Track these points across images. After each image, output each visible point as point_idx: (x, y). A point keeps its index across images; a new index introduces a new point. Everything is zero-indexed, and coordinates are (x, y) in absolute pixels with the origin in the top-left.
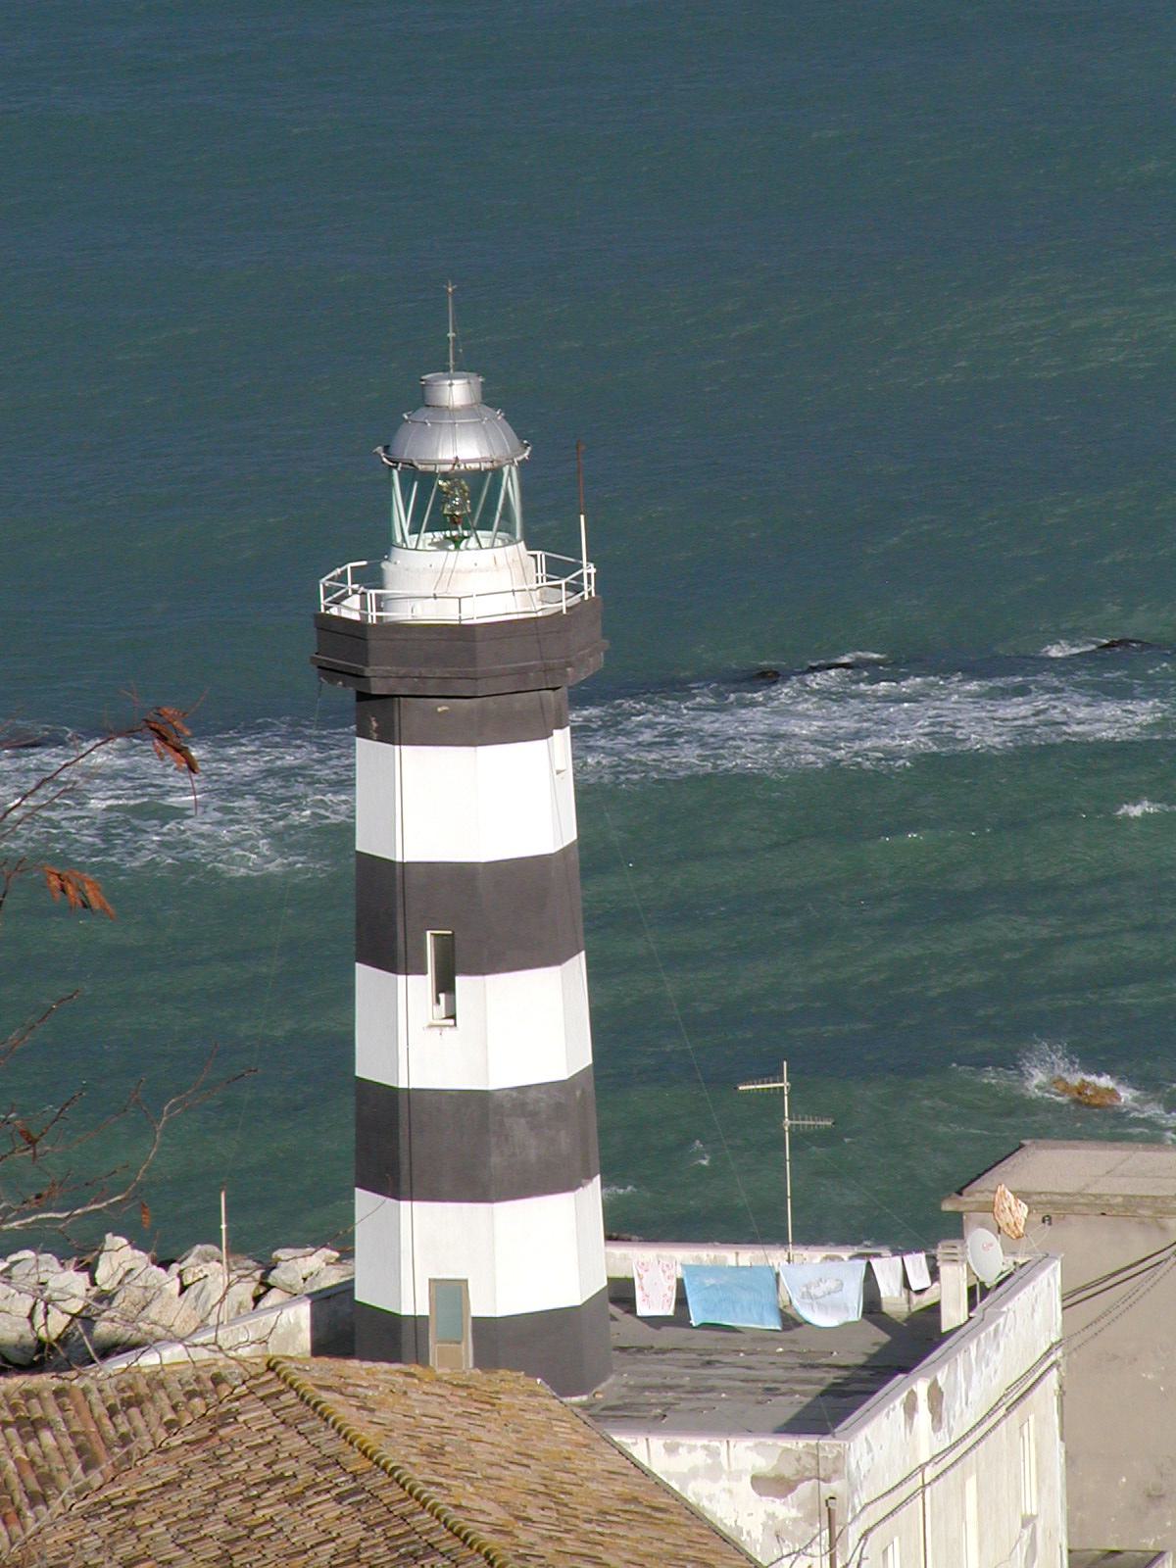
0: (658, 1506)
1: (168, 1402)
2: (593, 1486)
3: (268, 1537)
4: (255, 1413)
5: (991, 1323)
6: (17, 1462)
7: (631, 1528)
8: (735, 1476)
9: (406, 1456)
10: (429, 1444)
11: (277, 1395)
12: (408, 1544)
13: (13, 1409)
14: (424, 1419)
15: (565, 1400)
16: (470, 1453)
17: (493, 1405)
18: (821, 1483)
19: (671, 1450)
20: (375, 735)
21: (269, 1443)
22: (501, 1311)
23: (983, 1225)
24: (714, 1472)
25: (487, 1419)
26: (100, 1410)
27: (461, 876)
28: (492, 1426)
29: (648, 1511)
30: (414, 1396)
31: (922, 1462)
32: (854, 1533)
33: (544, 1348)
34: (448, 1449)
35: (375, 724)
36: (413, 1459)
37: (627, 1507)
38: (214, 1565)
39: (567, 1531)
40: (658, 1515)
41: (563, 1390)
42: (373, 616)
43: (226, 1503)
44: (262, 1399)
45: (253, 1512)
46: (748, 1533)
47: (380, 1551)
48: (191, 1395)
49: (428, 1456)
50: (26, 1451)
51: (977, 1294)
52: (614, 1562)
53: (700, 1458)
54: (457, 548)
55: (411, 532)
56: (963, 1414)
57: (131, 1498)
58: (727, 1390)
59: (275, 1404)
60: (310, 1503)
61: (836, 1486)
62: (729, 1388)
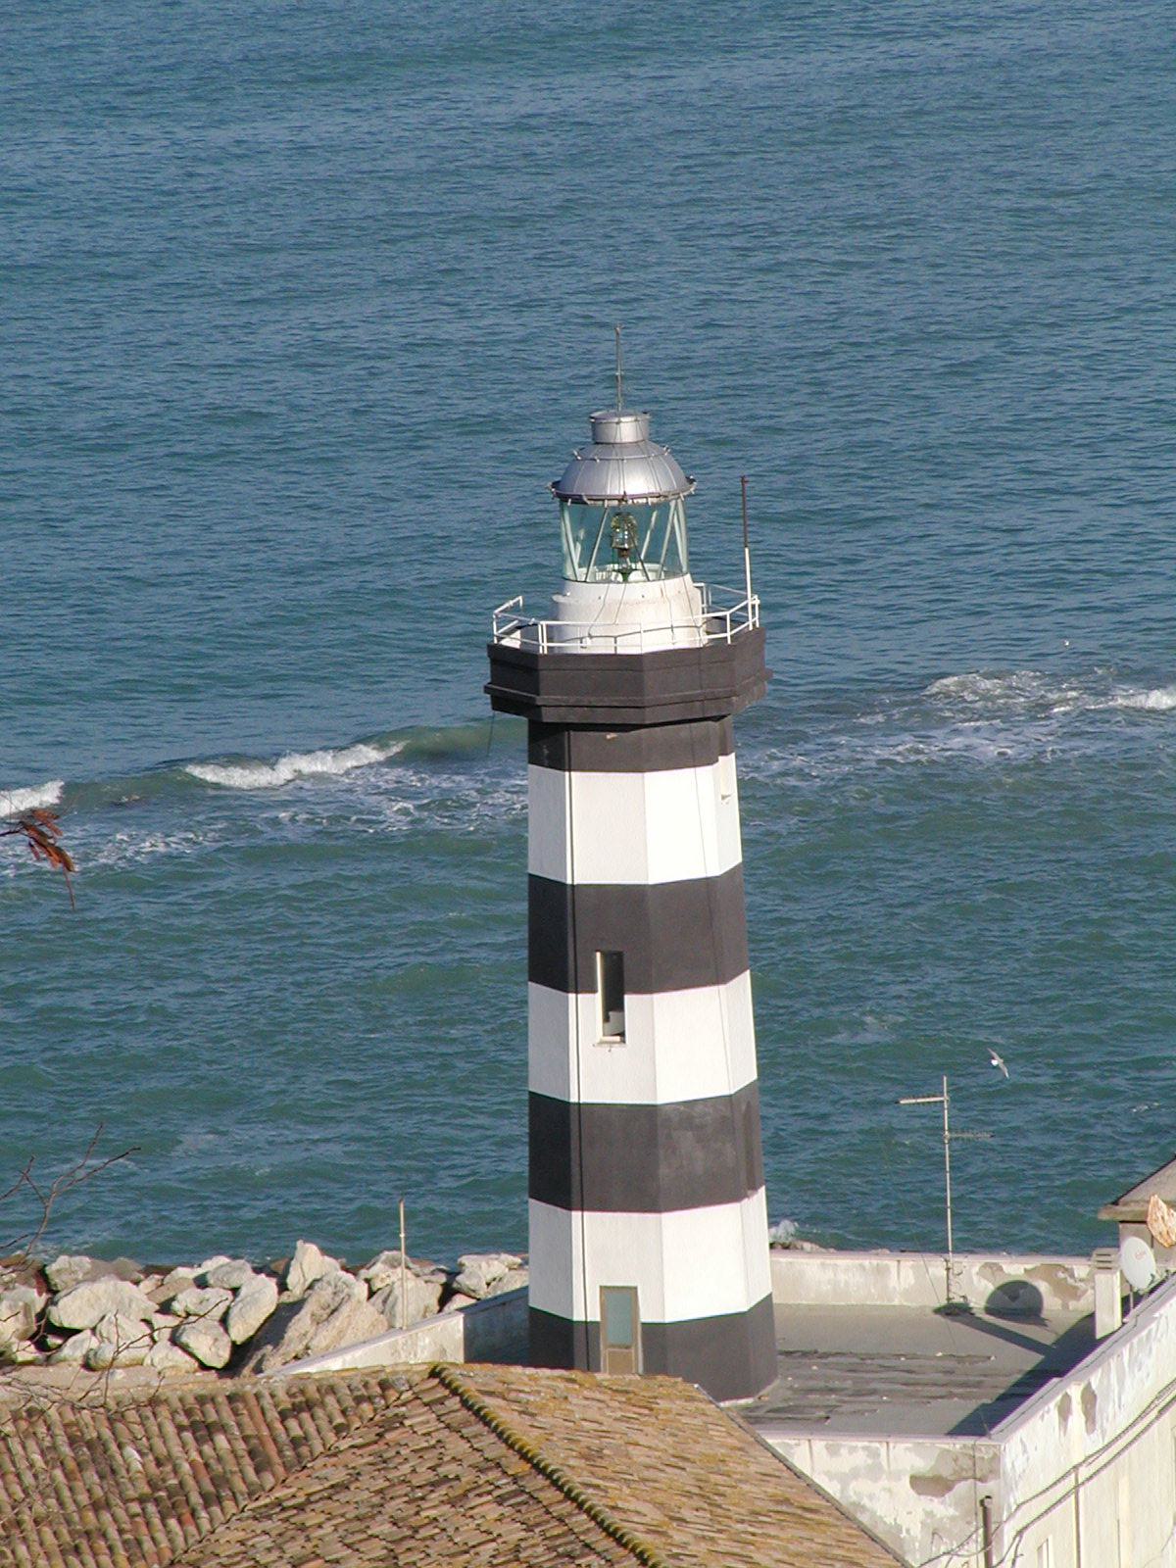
0: (805, 1505)
1: (337, 1406)
2: (746, 1487)
3: (432, 1537)
4: (420, 1418)
5: (1144, 1327)
6: (192, 1464)
7: (782, 1528)
8: (896, 1476)
9: (566, 1458)
10: (588, 1448)
11: (441, 1401)
12: (566, 1544)
13: (188, 1413)
14: (584, 1423)
15: (722, 1405)
16: (628, 1456)
17: (651, 1409)
18: (979, 1484)
19: (833, 1451)
20: (546, 762)
21: (434, 1447)
22: (670, 1317)
23: (1137, 1234)
24: (874, 1472)
25: (644, 1423)
26: (273, 1414)
27: (630, 899)
28: (649, 1430)
29: (799, 1512)
30: (575, 1401)
31: (1075, 1463)
32: (1009, 1531)
33: (720, 1355)
34: (606, 1452)
35: (546, 752)
36: (572, 1462)
37: (779, 1508)
38: (381, 1564)
39: (720, 1531)
40: (808, 1515)
41: (719, 1395)
42: (544, 646)
43: (393, 1503)
44: (426, 1405)
45: (417, 1513)
46: (908, 1531)
47: (540, 1550)
48: (359, 1400)
49: (587, 1459)
50: (201, 1453)
51: (1130, 1301)
52: (765, 1562)
53: (860, 1459)
54: (625, 580)
55: (580, 566)
56: (1116, 1416)
57: (301, 1499)
58: (889, 1393)
59: (438, 1408)
60: (473, 1504)
61: (989, 1487)
62: (890, 1391)
